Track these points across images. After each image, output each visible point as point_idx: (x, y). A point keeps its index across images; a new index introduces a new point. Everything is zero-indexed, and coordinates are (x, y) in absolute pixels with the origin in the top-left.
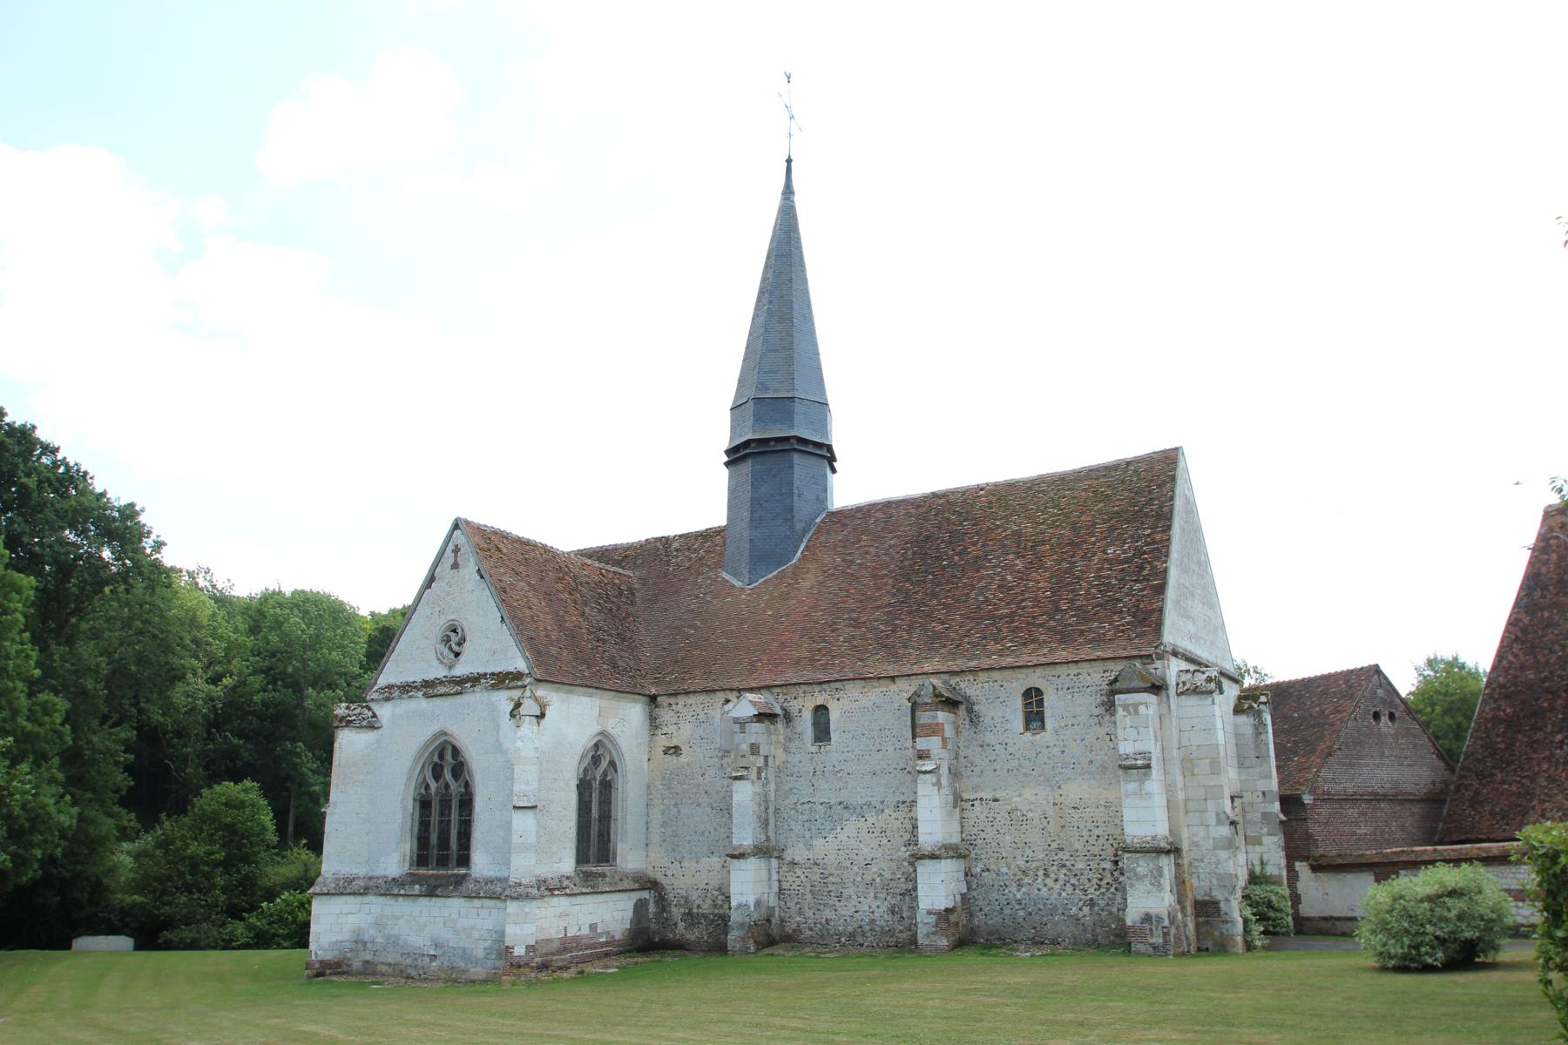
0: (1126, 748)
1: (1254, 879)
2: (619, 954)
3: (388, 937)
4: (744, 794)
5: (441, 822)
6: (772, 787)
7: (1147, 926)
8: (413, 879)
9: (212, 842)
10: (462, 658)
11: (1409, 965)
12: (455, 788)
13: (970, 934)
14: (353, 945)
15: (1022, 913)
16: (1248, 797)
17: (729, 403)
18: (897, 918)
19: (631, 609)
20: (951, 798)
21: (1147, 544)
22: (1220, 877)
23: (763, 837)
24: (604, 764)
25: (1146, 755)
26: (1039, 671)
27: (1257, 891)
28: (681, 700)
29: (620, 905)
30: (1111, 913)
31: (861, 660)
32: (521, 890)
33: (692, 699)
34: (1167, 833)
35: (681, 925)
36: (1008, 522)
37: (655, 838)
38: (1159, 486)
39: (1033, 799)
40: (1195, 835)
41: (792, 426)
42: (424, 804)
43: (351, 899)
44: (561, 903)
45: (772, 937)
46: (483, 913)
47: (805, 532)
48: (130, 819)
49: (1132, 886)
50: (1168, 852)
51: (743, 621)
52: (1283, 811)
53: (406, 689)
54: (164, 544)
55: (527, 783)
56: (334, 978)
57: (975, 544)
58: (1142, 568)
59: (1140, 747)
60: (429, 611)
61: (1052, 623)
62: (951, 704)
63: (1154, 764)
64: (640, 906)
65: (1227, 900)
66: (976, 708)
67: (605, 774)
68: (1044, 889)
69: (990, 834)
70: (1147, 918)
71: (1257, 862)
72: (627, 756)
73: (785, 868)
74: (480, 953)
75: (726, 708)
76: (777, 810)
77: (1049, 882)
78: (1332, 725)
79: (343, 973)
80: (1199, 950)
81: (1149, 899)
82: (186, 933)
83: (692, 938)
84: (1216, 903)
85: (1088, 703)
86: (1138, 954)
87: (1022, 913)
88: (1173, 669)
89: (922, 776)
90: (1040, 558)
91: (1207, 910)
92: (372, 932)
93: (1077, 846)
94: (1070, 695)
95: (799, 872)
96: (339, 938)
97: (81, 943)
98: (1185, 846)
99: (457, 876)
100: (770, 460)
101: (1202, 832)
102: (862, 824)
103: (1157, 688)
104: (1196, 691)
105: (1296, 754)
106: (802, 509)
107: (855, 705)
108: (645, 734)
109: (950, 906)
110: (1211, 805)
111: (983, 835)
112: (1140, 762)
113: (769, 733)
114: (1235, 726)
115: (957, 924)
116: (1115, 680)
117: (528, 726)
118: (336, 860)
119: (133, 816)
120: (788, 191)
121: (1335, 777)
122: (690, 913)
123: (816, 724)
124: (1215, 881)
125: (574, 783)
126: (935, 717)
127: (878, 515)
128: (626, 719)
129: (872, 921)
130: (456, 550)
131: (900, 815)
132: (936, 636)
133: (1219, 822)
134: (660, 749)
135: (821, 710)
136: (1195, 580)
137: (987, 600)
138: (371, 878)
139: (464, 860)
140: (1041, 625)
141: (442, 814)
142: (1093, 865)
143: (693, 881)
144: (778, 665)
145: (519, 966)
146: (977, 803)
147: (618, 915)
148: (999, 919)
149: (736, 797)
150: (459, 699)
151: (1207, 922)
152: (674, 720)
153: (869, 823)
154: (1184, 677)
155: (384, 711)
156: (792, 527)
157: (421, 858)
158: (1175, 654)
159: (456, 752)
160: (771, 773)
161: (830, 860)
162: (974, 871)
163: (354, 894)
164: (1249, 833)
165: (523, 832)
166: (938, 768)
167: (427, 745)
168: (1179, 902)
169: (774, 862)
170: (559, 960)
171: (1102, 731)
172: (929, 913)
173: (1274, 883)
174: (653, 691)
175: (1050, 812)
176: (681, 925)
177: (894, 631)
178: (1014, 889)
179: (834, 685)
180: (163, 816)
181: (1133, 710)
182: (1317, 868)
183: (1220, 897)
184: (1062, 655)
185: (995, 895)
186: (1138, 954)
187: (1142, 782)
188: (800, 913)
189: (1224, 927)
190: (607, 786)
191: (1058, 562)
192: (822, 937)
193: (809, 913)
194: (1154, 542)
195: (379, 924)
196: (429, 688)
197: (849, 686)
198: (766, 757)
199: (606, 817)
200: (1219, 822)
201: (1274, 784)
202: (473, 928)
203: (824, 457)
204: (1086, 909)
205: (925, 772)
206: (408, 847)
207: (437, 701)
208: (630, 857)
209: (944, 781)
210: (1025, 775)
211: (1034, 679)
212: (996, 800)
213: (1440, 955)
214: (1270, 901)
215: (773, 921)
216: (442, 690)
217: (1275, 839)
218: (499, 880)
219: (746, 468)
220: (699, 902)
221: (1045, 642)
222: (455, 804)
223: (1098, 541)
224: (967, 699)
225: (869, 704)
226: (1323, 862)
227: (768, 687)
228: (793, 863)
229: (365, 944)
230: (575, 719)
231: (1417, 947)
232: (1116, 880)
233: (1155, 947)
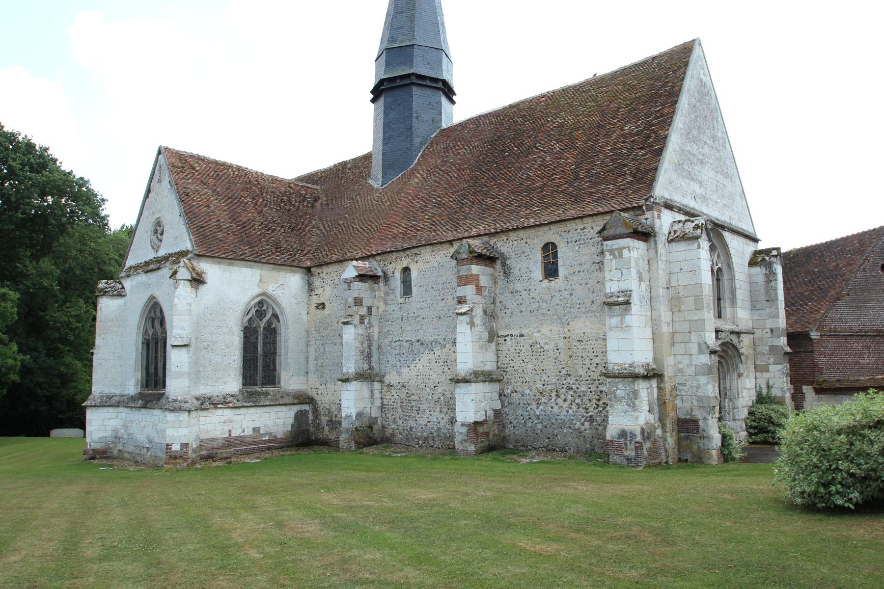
0: (612, 287)
1: (761, 399)
3: (128, 434)
4: (350, 334)
6: (376, 329)
7: (622, 441)
8: (141, 396)
11: (818, 506)
13: (496, 441)
14: (114, 439)
15: (539, 426)
16: (758, 333)
19: (310, 211)
20: (486, 335)
21: (656, 118)
22: (700, 399)
23: (366, 366)
25: (628, 293)
27: (762, 409)
28: (325, 269)
29: (282, 415)
31: (434, 231)
32: (176, 405)
34: (650, 360)
36: (556, 117)
37: (312, 368)
38: (675, 72)
40: (680, 363)
41: (411, 66)
43: (111, 409)
44: (227, 414)
45: (371, 437)
47: (421, 144)
49: (612, 406)
50: (646, 377)
52: (789, 345)
53: (136, 268)
55: (182, 328)
57: (530, 137)
58: (649, 137)
59: (623, 286)
61: (571, 189)
62: (487, 259)
63: (635, 299)
64: (300, 417)
65: (705, 419)
66: (508, 262)
67: (269, 323)
68: (556, 407)
69: (517, 363)
70: (623, 434)
71: (764, 386)
72: (287, 311)
73: (385, 389)
76: (379, 347)
77: (560, 401)
78: (843, 275)
80: (680, 460)
81: (631, 416)
84: (695, 422)
85: (588, 252)
86: (614, 464)
87: (539, 426)
88: (665, 222)
89: (460, 317)
90: (573, 140)
91: (688, 427)
94: (575, 245)
96: (105, 435)
97: (55, 433)
98: (668, 372)
100: (397, 92)
101: (686, 361)
102: (431, 356)
103: (645, 235)
104: (684, 238)
105: (811, 300)
107: (427, 266)
108: (305, 295)
109: (480, 418)
110: (694, 337)
112: (621, 299)
113: (373, 290)
114: (750, 276)
115: (487, 434)
116: (604, 229)
121: (842, 317)
122: (331, 421)
124: (695, 403)
126: (470, 270)
127: (471, 126)
128: (286, 287)
129: (439, 429)
132: (489, 208)
133: (701, 351)
135: (406, 270)
136: (706, 150)
137: (528, 177)
138: (122, 396)
140: (562, 192)
142: (593, 388)
144: (383, 239)
145: (176, 458)
146: (508, 338)
147: (280, 422)
149: (345, 337)
151: (687, 437)
154: (677, 227)
155: (128, 284)
156: (411, 142)
158: (669, 206)
160: (374, 320)
161: (413, 383)
164: (758, 363)
166: (471, 310)
168: (660, 420)
169: (377, 386)
170: (223, 453)
172: (463, 425)
173: (777, 403)
174: (308, 264)
175: (561, 345)
176: (326, 428)
177: (461, 208)
178: (534, 407)
181: (617, 254)
182: (819, 391)
183: (699, 416)
184: (572, 213)
185: (520, 412)
187: (623, 316)
188: (395, 422)
189: (701, 442)
190: (271, 332)
191: (585, 142)
193: (400, 422)
194: (662, 115)
197: (423, 250)
198: (370, 309)
200: (701, 351)
201: (782, 322)
203: (439, 89)
204: (587, 424)
205: (461, 314)
208: (291, 380)
209: (478, 320)
211: (550, 235)
212: (522, 336)
213: (855, 495)
214: (771, 418)
215: (375, 427)
217: (780, 367)
220: (336, 413)
221: (562, 204)
223: (619, 121)
224: (502, 255)
226: (824, 386)
227: (373, 256)
228: (390, 386)
229: (119, 438)
230: (234, 286)
231: (826, 485)
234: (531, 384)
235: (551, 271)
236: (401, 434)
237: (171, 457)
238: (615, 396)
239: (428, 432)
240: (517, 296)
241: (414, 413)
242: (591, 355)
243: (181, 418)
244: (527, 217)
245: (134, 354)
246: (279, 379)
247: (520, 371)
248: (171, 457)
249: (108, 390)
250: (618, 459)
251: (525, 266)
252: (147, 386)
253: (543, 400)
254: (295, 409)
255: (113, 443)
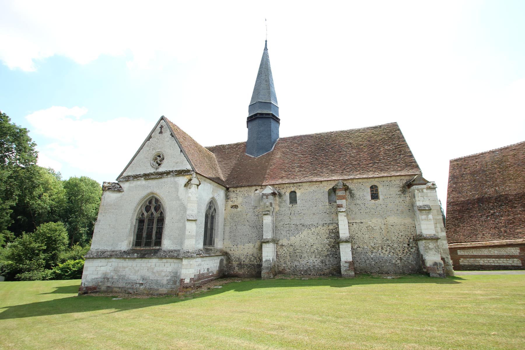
2: (215, 279)
3: (120, 276)
4: (268, 220)
5: (148, 228)
7: (436, 267)
9: (42, 243)
10: (162, 166)
12: (156, 215)
15: (373, 263)
17: (249, 104)
18: (324, 264)
24: (212, 209)
26: (376, 179)
28: (238, 189)
30: (408, 262)
33: (243, 189)
35: (237, 268)
37: (227, 237)
39: (376, 222)
42: (141, 221)
43: (103, 260)
46: (167, 265)
48: (10, 234)
51: (257, 167)
54: (36, 145)
56: (93, 295)
60: (148, 149)
64: (221, 261)
66: (353, 192)
69: (360, 234)
70: (436, 264)
74: (165, 282)
75: (256, 192)
77: (383, 251)
79: (97, 292)
82: (26, 274)
83: (241, 273)
85: (395, 191)
86: (433, 277)
87: (373, 263)
89: (340, 213)
92: (112, 274)
93: (394, 239)
95: (284, 248)
96: (96, 277)
99: (155, 250)
102: (309, 231)
106: (273, 137)
108: (224, 201)
111: (357, 235)
117: (193, 188)
118: (97, 244)
119: (13, 233)
120: (266, 49)
122: (240, 264)
123: (290, 197)
125: (204, 214)
130: (161, 127)
131: (325, 228)
134: (229, 206)
135: (293, 193)
138: (113, 251)
139: (159, 242)
140: (371, 167)
141: (149, 225)
142: (401, 245)
143: (242, 252)
145: (187, 288)
146: (354, 224)
147: (215, 265)
148: (365, 265)
150: (160, 180)
152: (235, 196)
153: (312, 231)
156: (271, 140)
157: (138, 242)
159: (157, 200)
162: (354, 247)
163: (105, 258)
165: (183, 231)
167: (144, 198)
171: (401, 200)
172: (346, 262)
175: (383, 227)
176: (237, 268)
178: (370, 254)
179: (298, 184)
180: (24, 233)
186: (433, 277)
187: (427, 215)
190: (213, 217)
192: (294, 272)
193: (289, 263)
195: (116, 270)
196: (147, 176)
199: (212, 229)
202: (162, 271)
204: (399, 261)
205: (342, 212)
206: (132, 238)
207: (150, 181)
208: (219, 244)
210: (372, 214)
212: (362, 223)
216: (153, 177)
218: (175, 251)
219: (255, 123)
220: (244, 260)
222: (155, 221)
225: (312, 191)
228: (282, 245)
229: (108, 279)
232: (409, 251)
233: (440, 275)
234: (368, 244)
235: (375, 196)
236: (289, 269)
237: (184, 287)
238: (429, 248)
239: (307, 267)
240: (358, 206)
241: (298, 259)
242: (398, 232)
243: (191, 263)
244: (293, 179)
245: (129, 226)
246: (214, 242)
247: (361, 238)
248: (184, 287)
249: (102, 248)
250: (435, 275)
251: (362, 194)
252: (136, 246)
253: (375, 251)
254: (220, 258)
255: (101, 282)
